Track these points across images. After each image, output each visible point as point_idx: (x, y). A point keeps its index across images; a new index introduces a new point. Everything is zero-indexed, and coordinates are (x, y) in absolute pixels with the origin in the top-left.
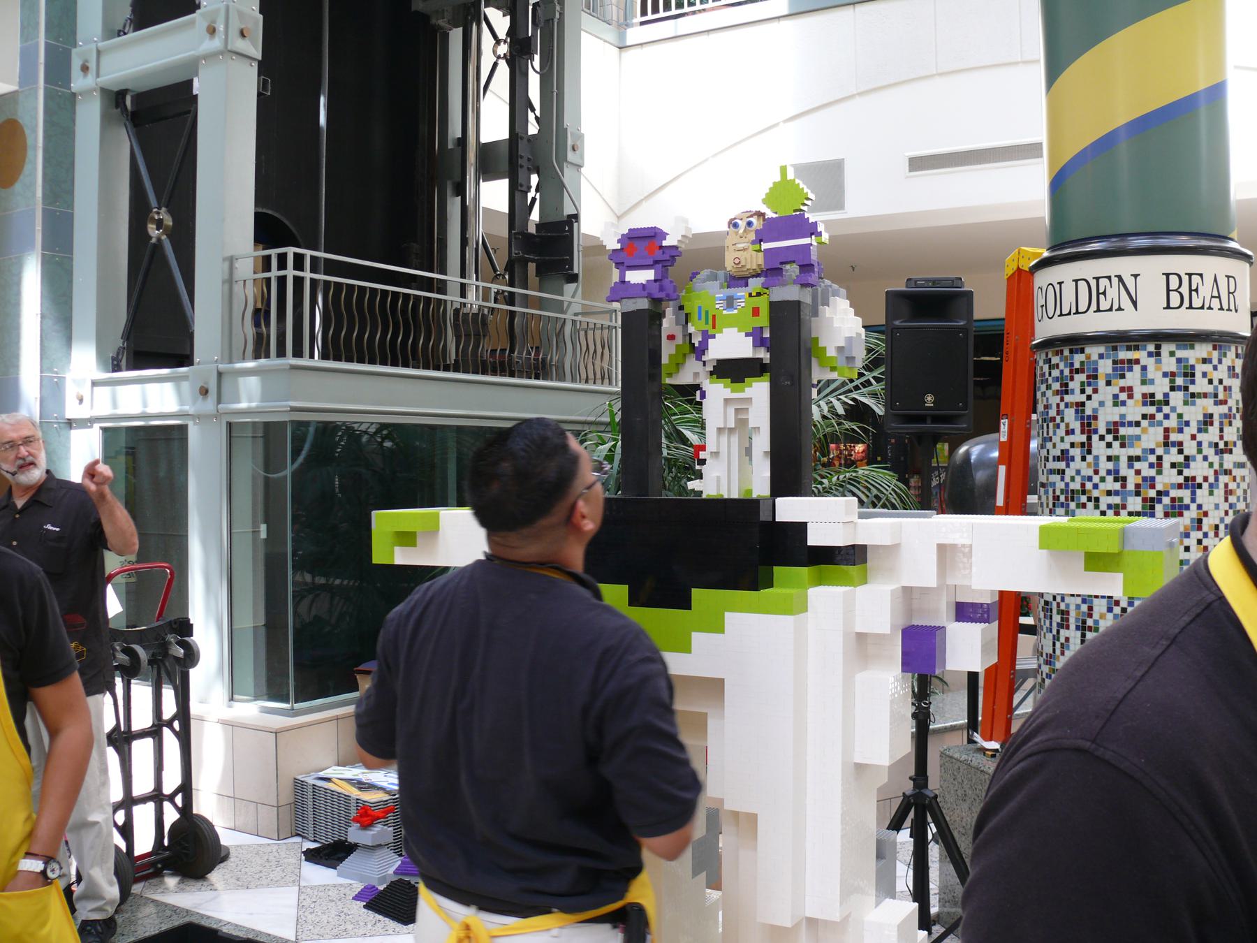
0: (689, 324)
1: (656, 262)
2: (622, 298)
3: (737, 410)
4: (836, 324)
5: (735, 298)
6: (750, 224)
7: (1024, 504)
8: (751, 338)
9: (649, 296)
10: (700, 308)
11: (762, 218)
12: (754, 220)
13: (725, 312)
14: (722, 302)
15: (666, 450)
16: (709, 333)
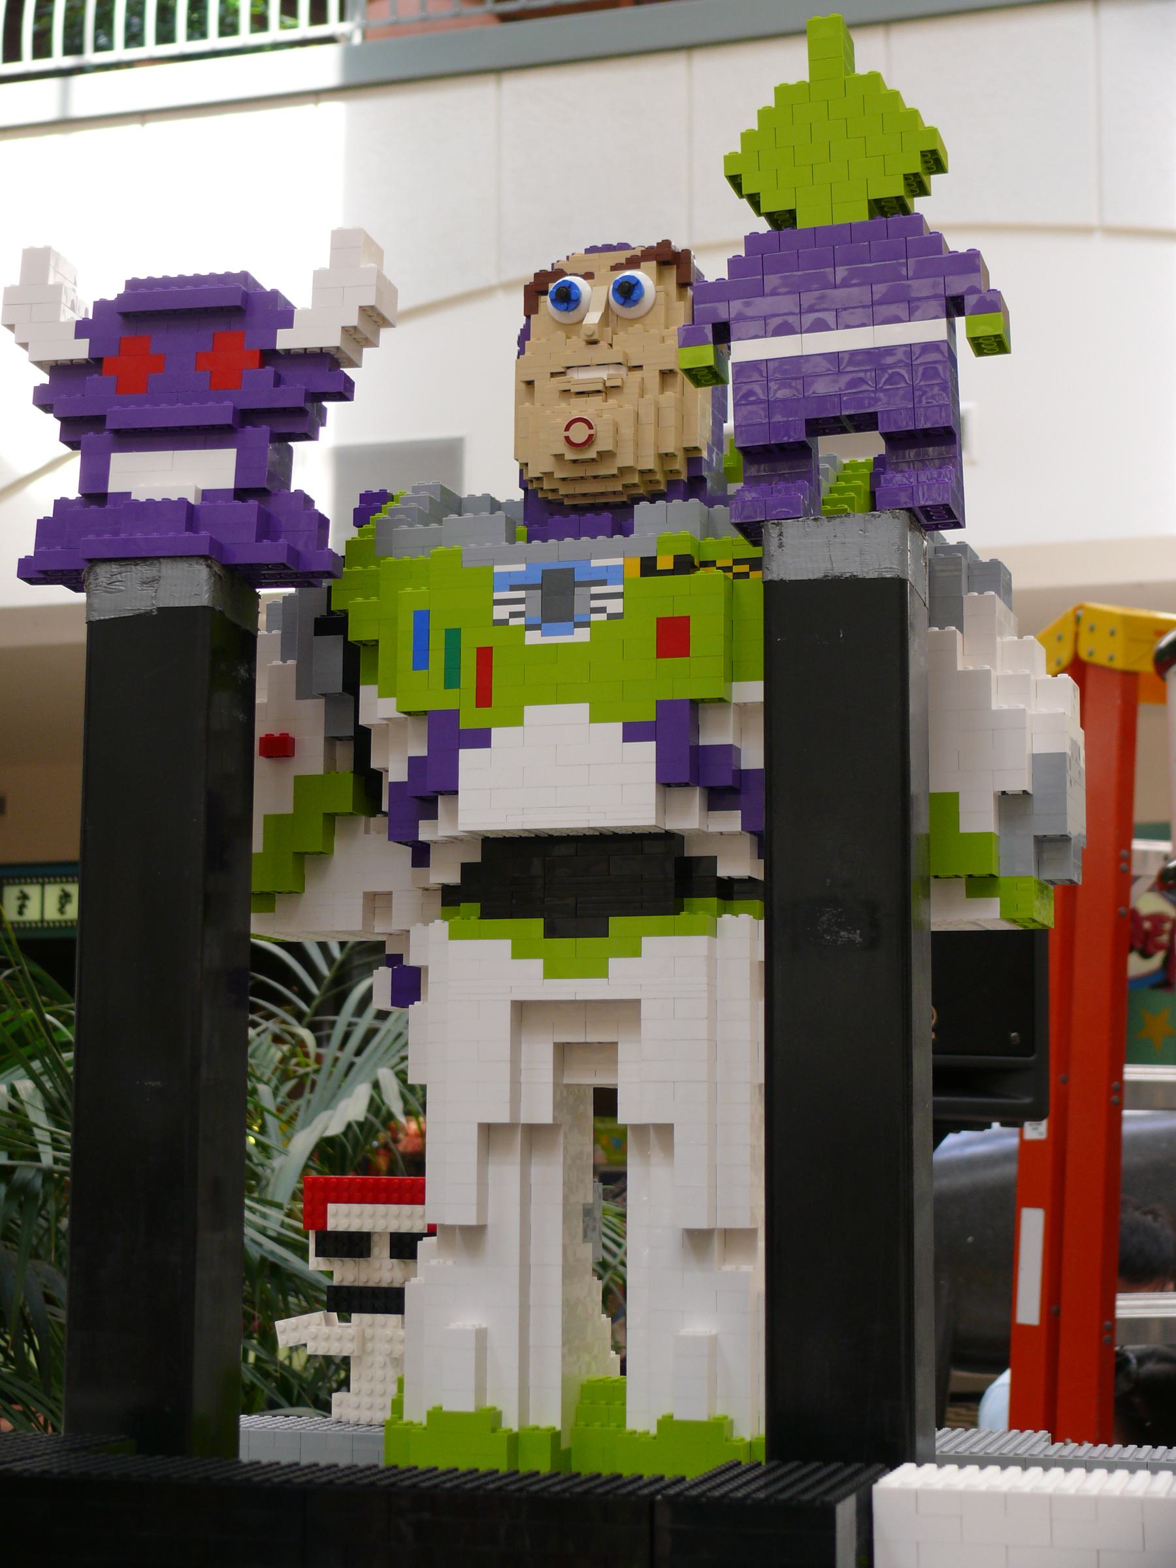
0: (367, 692)
1: (247, 417)
2: (94, 562)
3: (563, 1051)
4: (999, 702)
5: (578, 578)
6: (627, 292)
7: (1108, 1323)
8: (652, 745)
9: (214, 555)
10: (422, 620)
11: (672, 275)
12: (644, 276)
13: (533, 638)
14: (521, 594)
15: (49, 1149)
16: (463, 725)
